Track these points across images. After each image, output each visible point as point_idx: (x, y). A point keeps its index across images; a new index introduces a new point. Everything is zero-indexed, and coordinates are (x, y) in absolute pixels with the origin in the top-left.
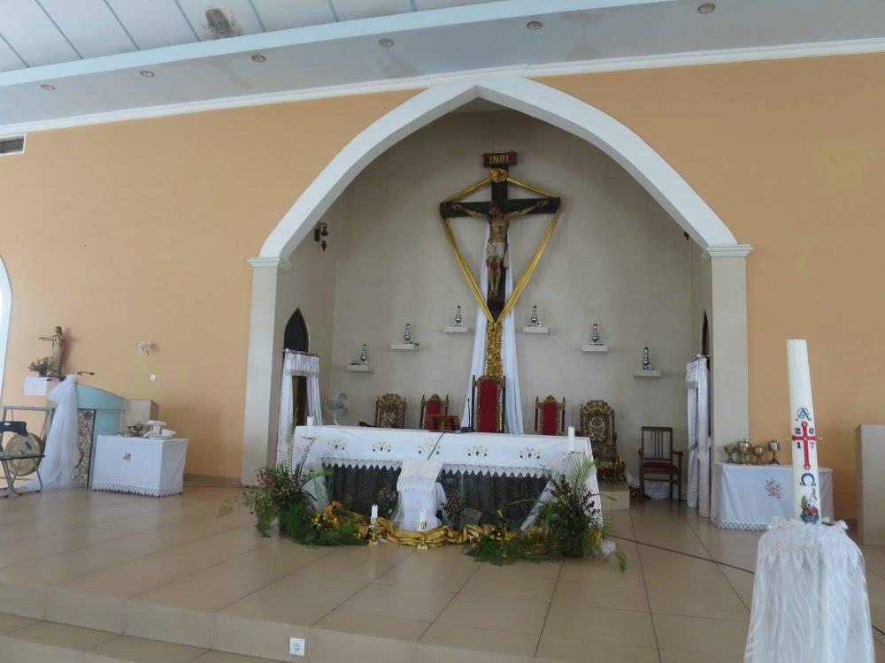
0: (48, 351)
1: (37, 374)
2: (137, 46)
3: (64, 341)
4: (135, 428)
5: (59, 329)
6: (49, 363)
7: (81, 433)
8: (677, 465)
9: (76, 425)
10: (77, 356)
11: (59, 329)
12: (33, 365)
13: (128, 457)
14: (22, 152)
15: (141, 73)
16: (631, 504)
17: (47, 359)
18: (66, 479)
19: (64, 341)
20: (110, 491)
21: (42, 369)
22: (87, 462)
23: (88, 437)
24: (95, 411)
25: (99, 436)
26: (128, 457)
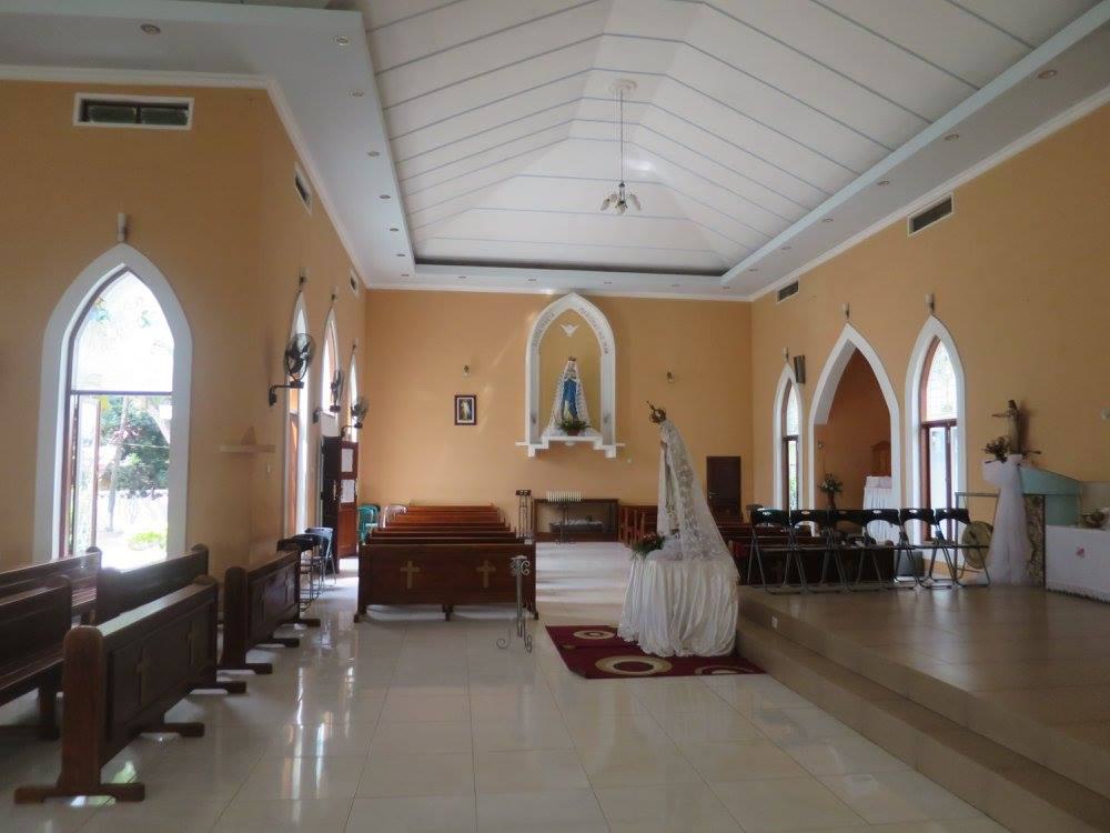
0: (1004, 429)
1: (993, 456)
2: (1027, 44)
3: (1020, 417)
4: (1092, 517)
5: (1012, 404)
6: (1006, 443)
7: (1030, 523)
8: (33, 695)
9: (1023, 510)
10: (1038, 433)
11: (1012, 404)
12: (988, 446)
13: (1081, 552)
14: (952, 213)
15: (1041, 76)
16: (357, 10)
17: (1001, 438)
18: (1018, 576)
19: (1020, 417)
20: (1077, 596)
21: (998, 451)
22: (1041, 557)
23: (1039, 527)
24: (1044, 496)
25: (343, 450)
26: (1081, 552)
